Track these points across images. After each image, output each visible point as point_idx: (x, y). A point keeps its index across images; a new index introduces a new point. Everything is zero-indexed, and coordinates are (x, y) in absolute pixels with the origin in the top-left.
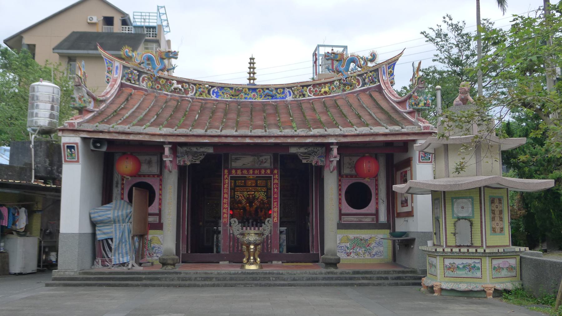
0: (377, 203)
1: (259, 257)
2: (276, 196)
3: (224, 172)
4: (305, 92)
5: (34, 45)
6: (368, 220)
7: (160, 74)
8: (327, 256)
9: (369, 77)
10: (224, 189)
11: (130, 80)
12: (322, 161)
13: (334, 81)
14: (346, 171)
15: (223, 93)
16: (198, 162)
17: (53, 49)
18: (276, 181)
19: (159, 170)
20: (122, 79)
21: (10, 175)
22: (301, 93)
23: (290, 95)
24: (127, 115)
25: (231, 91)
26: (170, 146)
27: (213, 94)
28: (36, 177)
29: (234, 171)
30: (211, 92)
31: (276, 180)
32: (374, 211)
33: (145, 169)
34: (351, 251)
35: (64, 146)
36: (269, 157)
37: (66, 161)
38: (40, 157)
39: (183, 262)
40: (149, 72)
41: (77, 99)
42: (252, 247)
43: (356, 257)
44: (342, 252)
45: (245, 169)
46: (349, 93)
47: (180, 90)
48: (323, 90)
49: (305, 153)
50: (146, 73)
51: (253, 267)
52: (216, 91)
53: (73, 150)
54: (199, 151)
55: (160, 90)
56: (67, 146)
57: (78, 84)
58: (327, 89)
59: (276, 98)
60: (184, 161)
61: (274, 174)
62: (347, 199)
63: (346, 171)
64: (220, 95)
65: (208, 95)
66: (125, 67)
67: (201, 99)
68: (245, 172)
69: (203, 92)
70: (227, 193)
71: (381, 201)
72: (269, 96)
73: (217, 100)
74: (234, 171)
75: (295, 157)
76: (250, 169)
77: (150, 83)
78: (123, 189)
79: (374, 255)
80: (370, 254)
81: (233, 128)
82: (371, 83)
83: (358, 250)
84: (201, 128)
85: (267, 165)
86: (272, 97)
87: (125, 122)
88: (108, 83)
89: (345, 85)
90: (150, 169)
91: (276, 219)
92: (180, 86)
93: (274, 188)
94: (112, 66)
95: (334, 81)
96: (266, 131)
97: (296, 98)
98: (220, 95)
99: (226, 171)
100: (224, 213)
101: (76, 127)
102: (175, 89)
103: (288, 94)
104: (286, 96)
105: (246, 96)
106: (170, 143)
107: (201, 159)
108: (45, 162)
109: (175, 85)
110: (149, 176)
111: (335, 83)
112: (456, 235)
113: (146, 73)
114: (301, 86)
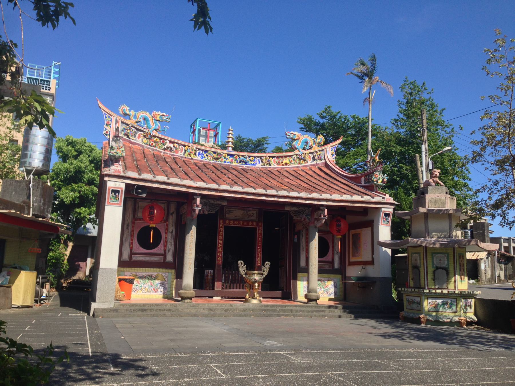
0: (333, 254)
2: (260, 244)
7: (155, 133)
10: (219, 235)
13: (292, 155)
15: (207, 156)
16: (214, 212)
18: (260, 232)
23: (259, 162)
25: (214, 155)
29: (227, 222)
30: (197, 154)
32: (162, 252)
35: (109, 189)
36: (255, 212)
37: (109, 203)
40: (145, 130)
42: (256, 284)
45: (236, 220)
46: (303, 166)
47: (171, 148)
48: (284, 162)
49: (295, 211)
51: (255, 302)
52: (201, 152)
54: (215, 203)
55: (154, 146)
56: (112, 190)
57: (117, 135)
58: (287, 161)
59: (249, 164)
67: (189, 159)
68: (237, 223)
70: (222, 240)
72: (243, 162)
74: (227, 222)
76: (241, 220)
78: (133, 231)
79: (330, 294)
86: (246, 163)
89: (300, 160)
94: (111, 121)
95: (292, 155)
97: (264, 165)
99: (221, 221)
100: (219, 256)
101: (122, 174)
102: (168, 148)
103: (258, 162)
108: (40, 202)
109: (168, 144)
111: (293, 157)
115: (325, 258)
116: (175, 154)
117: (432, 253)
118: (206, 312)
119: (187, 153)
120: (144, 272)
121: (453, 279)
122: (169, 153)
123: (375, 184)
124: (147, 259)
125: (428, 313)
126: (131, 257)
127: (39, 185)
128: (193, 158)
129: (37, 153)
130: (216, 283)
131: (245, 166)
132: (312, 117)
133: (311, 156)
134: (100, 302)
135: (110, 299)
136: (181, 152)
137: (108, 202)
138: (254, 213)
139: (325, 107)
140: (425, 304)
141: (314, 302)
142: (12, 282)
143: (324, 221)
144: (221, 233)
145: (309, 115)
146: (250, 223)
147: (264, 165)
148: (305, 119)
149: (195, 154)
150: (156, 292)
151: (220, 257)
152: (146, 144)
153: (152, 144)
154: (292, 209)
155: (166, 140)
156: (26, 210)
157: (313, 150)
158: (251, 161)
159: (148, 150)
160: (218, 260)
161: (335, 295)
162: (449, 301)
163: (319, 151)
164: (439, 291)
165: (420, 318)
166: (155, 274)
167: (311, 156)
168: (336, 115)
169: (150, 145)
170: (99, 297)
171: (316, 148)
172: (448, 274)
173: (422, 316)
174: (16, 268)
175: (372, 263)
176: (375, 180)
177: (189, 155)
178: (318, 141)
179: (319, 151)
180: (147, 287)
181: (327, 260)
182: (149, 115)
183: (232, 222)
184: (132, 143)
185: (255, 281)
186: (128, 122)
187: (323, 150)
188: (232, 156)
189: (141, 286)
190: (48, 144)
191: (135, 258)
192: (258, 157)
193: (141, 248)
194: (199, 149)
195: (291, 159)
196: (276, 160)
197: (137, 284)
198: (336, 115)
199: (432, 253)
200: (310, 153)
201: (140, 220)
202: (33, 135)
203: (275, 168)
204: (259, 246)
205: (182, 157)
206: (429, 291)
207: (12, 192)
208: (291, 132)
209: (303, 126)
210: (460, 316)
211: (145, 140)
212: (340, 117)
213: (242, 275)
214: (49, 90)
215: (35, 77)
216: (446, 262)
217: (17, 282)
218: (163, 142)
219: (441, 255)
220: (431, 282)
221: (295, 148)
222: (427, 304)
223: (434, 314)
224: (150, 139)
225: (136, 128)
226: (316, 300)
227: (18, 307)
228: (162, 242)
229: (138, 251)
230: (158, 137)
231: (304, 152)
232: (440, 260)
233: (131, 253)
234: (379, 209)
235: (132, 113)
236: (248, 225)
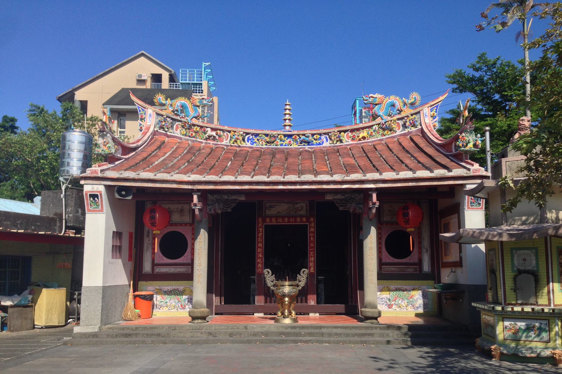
0: (420, 253)
1: (294, 309)
2: (312, 245)
3: (258, 220)
4: (342, 138)
5: (86, 102)
6: (410, 270)
7: (195, 121)
8: (368, 311)
10: (258, 237)
11: (163, 128)
12: (360, 208)
13: (373, 126)
14: (386, 218)
15: (258, 140)
16: (229, 210)
17: (103, 105)
18: (312, 230)
20: (154, 128)
21: (38, 226)
23: (327, 140)
24: (156, 163)
25: (266, 138)
26: (199, 194)
27: (248, 142)
28: (67, 227)
29: (268, 220)
30: (246, 140)
31: (312, 229)
32: (416, 261)
33: (176, 218)
34: (393, 303)
35: (86, 194)
36: (305, 204)
37: (89, 210)
38: (71, 207)
39: (216, 314)
40: (183, 120)
41: (102, 146)
42: (287, 299)
43: (398, 309)
44: (383, 304)
46: (388, 138)
47: (215, 137)
48: (361, 135)
50: (180, 121)
51: (287, 321)
53: (96, 199)
55: (194, 137)
57: (102, 130)
59: (312, 145)
60: (215, 210)
61: (310, 223)
62: (386, 245)
63: (386, 218)
64: (255, 142)
65: (242, 142)
66: (158, 114)
67: (236, 146)
69: (238, 139)
70: (262, 243)
71: (424, 250)
72: (305, 142)
73: (251, 148)
74: (268, 220)
75: (331, 203)
77: (184, 130)
79: (418, 308)
80: (413, 306)
81: (264, 175)
82: (412, 126)
83: (400, 302)
85: (303, 212)
86: (308, 143)
87: (157, 169)
88: (141, 131)
89: (384, 130)
90: (182, 218)
91: (312, 269)
92: (214, 133)
93: (310, 237)
95: (373, 126)
96: (299, 177)
97: (333, 143)
99: (260, 220)
101: (100, 175)
102: (210, 136)
103: (325, 140)
104: (323, 142)
105: (282, 142)
106: (199, 190)
107: (232, 207)
108: (77, 212)
109: (210, 132)
110: (181, 225)
111: (374, 127)
112: (517, 291)
113: (180, 121)
114: (338, 131)
115: (408, 258)
116: (219, 143)
118: (205, 337)
119: (233, 140)
120: (169, 286)
121: (546, 288)
122: (211, 142)
123: (463, 151)
124: (172, 270)
125: (503, 344)
126: (153, 269)
127: (73, 194)
128: (240, 144)
129: (75, 159)
130: (256, 297)
131: (307, 147)
132: (463, 71)
133: (401, 122)
134: (84, 325)
135: (95, 322)
136: (227, 140)
138: (302, 206)
139: (477, 56)
140: (499, 329)
143: (374, 211)
144: (260, 234)
145: (459, 69)
146: (298, 220)
147: (333, 143)
148: (454, 75)
149: (244, 140)
150: (184, 308)
151: (260, 265)
152: (185, 135)
153: (192, 134)
154: (335, 197)
155: (207, 127)
156: (58, 222)
157: (403, 114)
158: (315, 140)
159: (187, 142)
160: (258, 268)
161: (424, 309)
162: (537, 325)
163: (412, 115)
164: (518, 309)
165: (490, 350)
166: (181, 288)
167: (401, 122)
168: (495, 64)
169: (189, 136)
170: (83, 319)
171: (407, 111)
172: (537, 281)
173: (493, 347)
175: (459, 264)
176: (461, 145)
177: (236, 142)
178: (410, 102)
179: (412, 115)
180: (173, 304)
181: (412, 261)
183: (274, 220)
184: (168, 136)
185: (284, 296)
186: (163, 113)
187: (419, 112)
188: (290, 136)
189: (166, 302)
191: (158, 270)
192: (325, 134)
193: (164, 258)
194: (247, 134)
195: (372, 131)
196: (350, 134)
197: (162, 300)
198: (495, 64)
199: (512, 249)
200: (398, 119)
201: (176, 226)
202: (69, 141)
204: (311, 247)
206: (503, 308)
207: (50, 204)
208: (371, 95)
209: (455, 86)
210: (554, 349)
211: (184, 132)
212: (501, 64)
213: (269, 288)
214: (202, 93)
215: (188, 82)
216: (534, 262)
217: (39, 301)
218: (205, 130)
219: (526, 251)
221: (376, 115)
222: (503, 330)
223: (513, 345)
224: (189, 129)
225: (172, 119)
226: (376, 318)
227: (42, 328)
228: (189, 249)
229: (162, 262)
230: (198, 126)
231: (389, 118)
232: (525, 260)
233: (154, 265)
234: (463, 185)
235: (169, 102)
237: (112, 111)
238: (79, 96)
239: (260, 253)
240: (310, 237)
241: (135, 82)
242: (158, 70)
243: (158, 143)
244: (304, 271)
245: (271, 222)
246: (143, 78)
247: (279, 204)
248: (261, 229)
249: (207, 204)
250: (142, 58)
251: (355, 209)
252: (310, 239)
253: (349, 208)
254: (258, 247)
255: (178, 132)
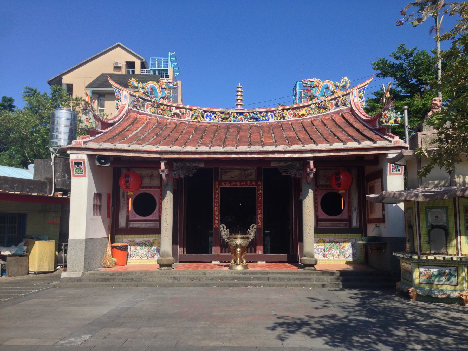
0: (350, 211)
2: (260, 205)
3: (215, 184)
4: (285, 115)
5: (72, 85)
6: (342, 225)
7: (162, 101)
8: (306, 260)
9: (341, 101)
10: (215, 198)
11: (136, 107)
12: (300, 174)
14: (322, 182)
15: (215, 117)
16: (191, 175)
17: (86, 87)
18: (260, 191)
19: (159, 184)
21: (31, 188)
22: (281, 116)
23: (272, 117)
24: (130, 136)
25: (222, 115)
26: (166, 161)
27: (207, 118)
28: (56, 190)
29: (223, 183)
30: (205, 116)
31: (260, 191)
32: (347, 218)
34: (327, 252)
35: (72, 162)
36: (254, 171)
37: (74, 176)
39: (180, 262)
40: (152, 100)
41: (85, 121)
42: (239, 250)
43: (331, 258)
44: (319, 254)
46: (323, 115)
47: (179, 114)
48: (301, 113)
50: (150, 101)
51: (239, 268)
53: (80, 166)
55: (162, 114)
57: (85, 108)
59: (260, 121)
60: (179, 175)
61: (258, 186)
63: (322, 182)
64: (213, 119)
65: (202, 119)
66: (131, 95)
67: (196, 122)
69: (198, 116)
70: (218, 202)
71: (353, 208)
72: (254, 119)
73: (209, 123)
74: (223, 183)
75: (276, 170)
77: (153, 108)
79: (348, 257)
80: (344, 255)
81: (220, 146)
82: (343, 105)
83: (333, 252)
84: (193, 146)
85: (252, 177)
86: (257, 119)
87: (130, 141)
88: (117, 109)
89: (320, 108)
90: (152, 182)
92: (178, 111)
93: (258, 198)
96: (249, 148)
97: (277, 119)
98: (213, 119)
99: (217, 183)
101: (83, 146)
102: (174, 114)
103: (270, 117)
104: (269, 119)
105: (235, 119)
106: (165, 159)
107: (193, 173)
108: (64, 177)
109: (175, 110)
110: (151, 187)
111: (311, 106)
112: (431, 243)
113: (150, 101)
114: (281, 110)
115: (340, 215)
116: (182, 119)
117: (426, 208)
118: (170, 281)
119: (194, 117)
120: (141, 238)
121: (455, 241)
122: (176, 119)
123: (385, 126)
125: (418, 287)
126: (127, 225)
127: (61, 162)
129: (63, 133)
130: (213, 248)
131: (255, 123)
132: (385, 60)
133: (334, 102)
136: (189, 117)
137: (73, 174)
138: (252, 172)
139: (398, 46)
140: (416, 274)
141: (312, 268)
142: (29, 251)
143: (311, 176)
144: (217, 196)
145: (382, 58)
147: (277, 119)
148: (378, 63)
149: (203, 117)
150: (153, 257)
151: (216, 221)
152: (154, 113)
153: (160, 112)
154: (279, 165)
155: (172, 106)
156: (48, 185)
157: (336, 96)
158: (263, 117)
160: (215, 223)
161: (353, 257)
162: (447, 271)
163: (343, 96)
164: (431, 258)
165: (408, 292)
166: (151, 240)
167: (334, 102)
168: (412, 53)
169: (158, 114)
170: (69, 266)
171: (339, 93)
172: (447, 234)
173: (410, 290)
174: (32, 238)
175: (382, 220)
176: (384, 121)
177: (197, 118)
178: (341, 85)
179: (343, 96)
180: (144, 253)
182: (157, 85)
183: (228, 183)
185: (237, 247)
186: (136, 94)
187: (349, 94)
188: (241, 114)
189: (139, 252)
190: (71, 124)
191: (132, 225)
192: (270, 112)
194: (206, 112)
195: (309, 109)
196: (291, 112)
197: (135, 250)
198: (412, 53)
199: (426, 208)
200: (332, 99)
201: (147, 188)
202: (58, 117)
203: (290, 121)
204: (259, 206)
205: (189, 122)
206: (419, 257)
207: (42, 170)
208: (309, 79)
209: (379, 72)
210: (461, 291)
212: (417, 53)
213: (224, 240)
214: (168, 77)
215: (156, 68)
216: (445, 219)
218: (170, 109)
219: (438, 210)
220: (425, 245)
221: (313, 96)
222: (419, 275)
223: (427, 288)
224: (157, 108)
225: (143, 99)
226: (313, 266)
227: (35, 273)
229: (135, 218)
231: (324, 99)
233: (128, 221)
234: (386, 155)
236: (246, 185)
237: (94, 93)
238: (66, 80)
239: (216, 211)
240: (258, 198)
241: (113, 68)
242: (131, 58)
243: (131, 120)
244: (253, 226)
245: (225, 185)
246: (119, 65)
247: (233, 170)
248: (217, 191)
249: (173, 171)
250: (119, 49)
251: (295, 175)
252: (258, 199)
253: (291, 174)
254: (215, 206)
255: (148, 110)
